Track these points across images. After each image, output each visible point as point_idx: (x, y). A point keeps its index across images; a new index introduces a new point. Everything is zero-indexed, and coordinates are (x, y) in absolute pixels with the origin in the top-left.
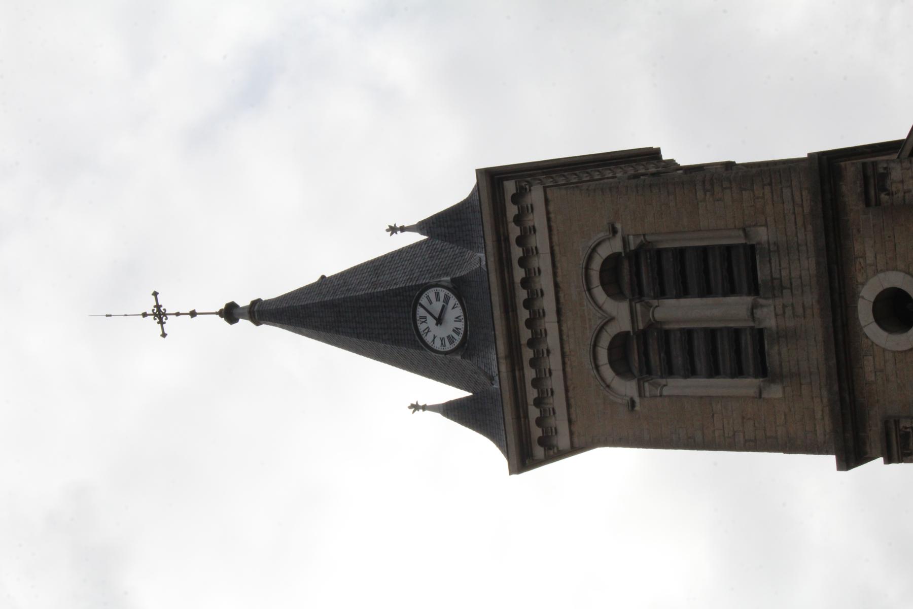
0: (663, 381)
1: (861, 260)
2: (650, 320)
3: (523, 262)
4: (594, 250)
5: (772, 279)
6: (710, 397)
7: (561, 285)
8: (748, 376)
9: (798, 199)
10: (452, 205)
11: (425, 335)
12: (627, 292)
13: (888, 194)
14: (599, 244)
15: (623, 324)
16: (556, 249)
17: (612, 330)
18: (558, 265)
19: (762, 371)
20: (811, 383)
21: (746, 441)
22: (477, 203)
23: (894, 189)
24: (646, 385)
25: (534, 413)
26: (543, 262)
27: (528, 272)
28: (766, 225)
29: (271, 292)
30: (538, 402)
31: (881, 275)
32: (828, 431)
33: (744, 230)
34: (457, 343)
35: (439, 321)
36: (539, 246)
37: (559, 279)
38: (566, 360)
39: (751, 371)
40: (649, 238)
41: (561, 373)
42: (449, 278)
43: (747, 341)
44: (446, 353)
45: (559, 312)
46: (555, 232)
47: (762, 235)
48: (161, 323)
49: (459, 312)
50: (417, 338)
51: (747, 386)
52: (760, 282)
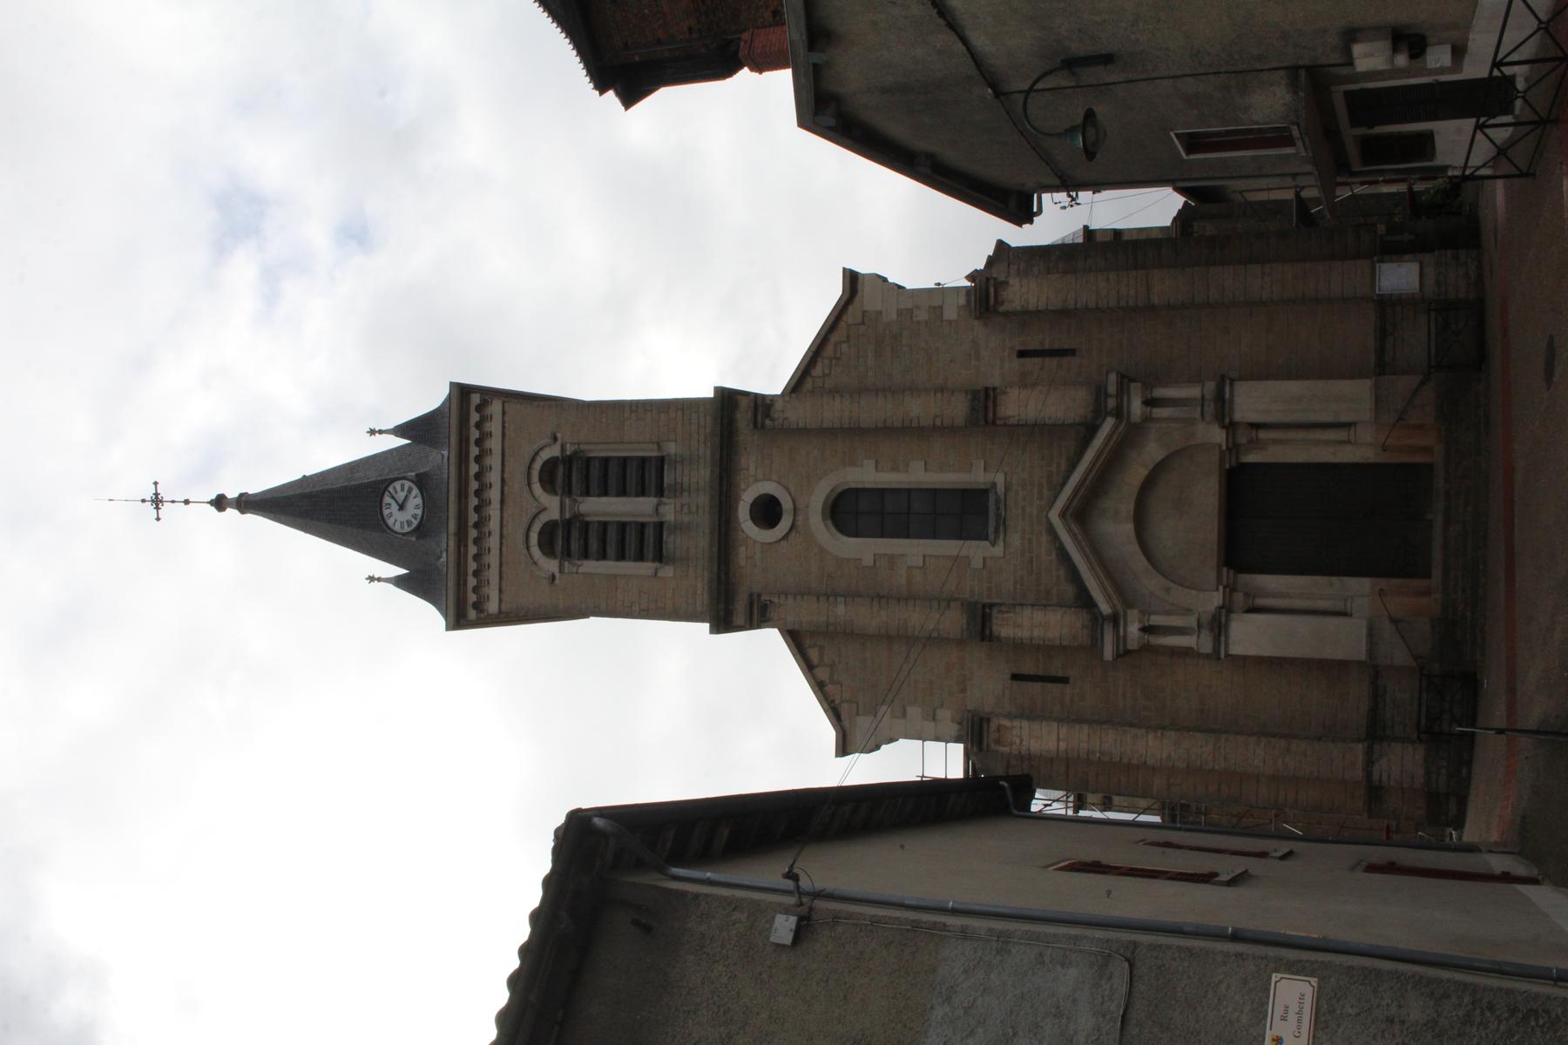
0: (579, 563)
1: (745, 472)
3: (478, 459)
4: (537, 453)
5: (676, 483)
6: (616, 576)
7: (506, 480)
8: (647, 561)
9: (702, 423)
10: (428, 411)
12: (559, 491)
13: (771, 420)
14: (541, 449)
15: (554, 514)
16: (507, 451)
17: (544, 518)
18: (506, 464)
19: (659, 557)
20: (696, 566)
21: (640, 611)
22: (447, 410)
23: (776, 417)
24: (566, 563)
25: (472, 582)
26: (494, 461)
27: (481, 468)
28: (676, 441)
29: (258, 485)
30: (476, 574)
31: (760, 484)
32: (705, 602)
33: (658, 444)
34: (414, 526)
35: (402, 507)
37: (506, 476)
39: (651, 556)
40: (582, 447)
41: (498, 551)
42: (414, 474)
43: (650, 534)
44: (404, 534)
45: (502, 502)
46: (507, 438)
47: (671, 448)
48: (157, 508)
49: (419, 501)
50: (382, 522)
51: (646, 568)
52: (665, 485)
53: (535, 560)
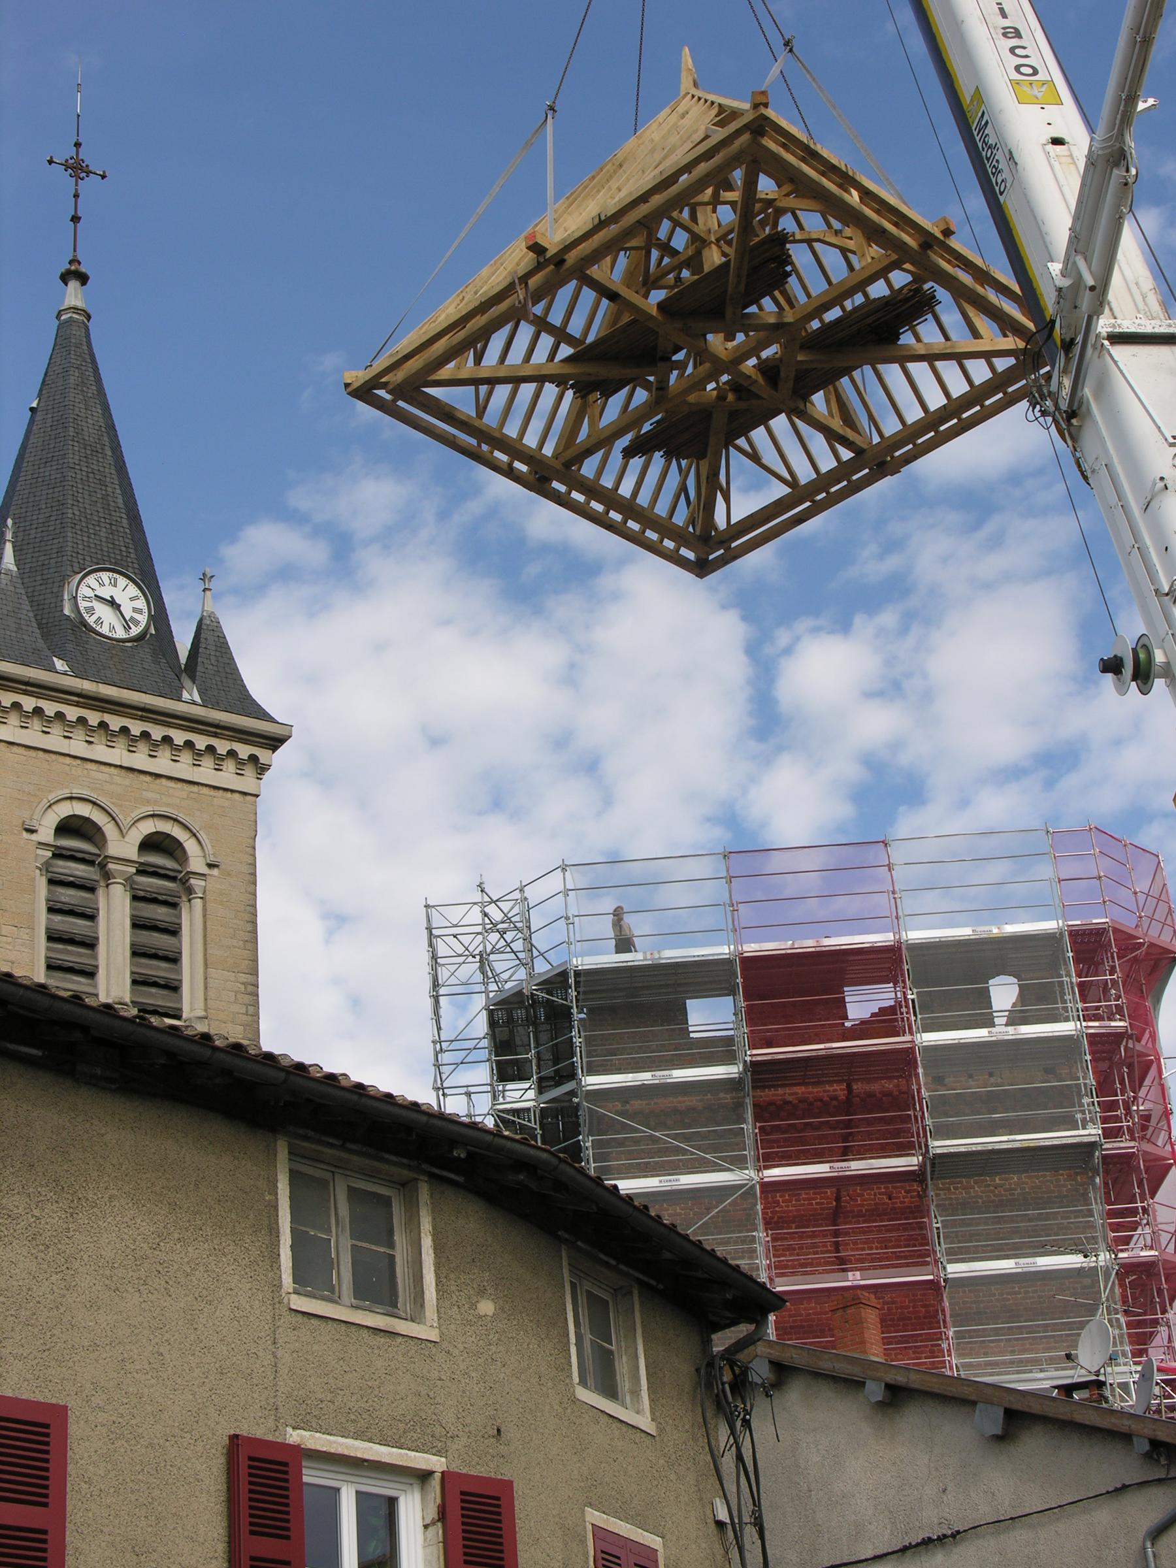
2: (115, 878)
11: (111, 576)
16: (195, 788)
17: (109, 830)
26: (184, 768)
36: (201, 769)
37: (164, 781)
38: (79, 762)
46: (213, 792)
53: (54, 807)
